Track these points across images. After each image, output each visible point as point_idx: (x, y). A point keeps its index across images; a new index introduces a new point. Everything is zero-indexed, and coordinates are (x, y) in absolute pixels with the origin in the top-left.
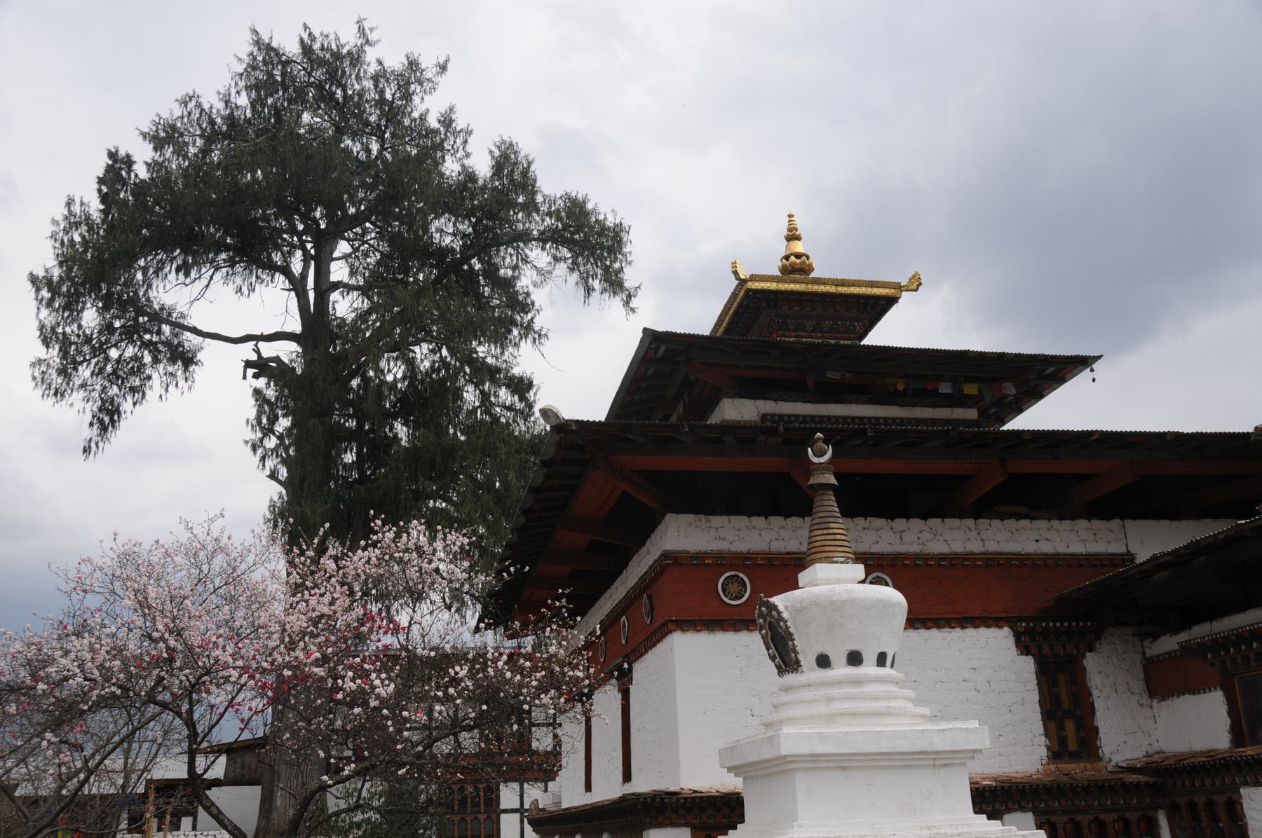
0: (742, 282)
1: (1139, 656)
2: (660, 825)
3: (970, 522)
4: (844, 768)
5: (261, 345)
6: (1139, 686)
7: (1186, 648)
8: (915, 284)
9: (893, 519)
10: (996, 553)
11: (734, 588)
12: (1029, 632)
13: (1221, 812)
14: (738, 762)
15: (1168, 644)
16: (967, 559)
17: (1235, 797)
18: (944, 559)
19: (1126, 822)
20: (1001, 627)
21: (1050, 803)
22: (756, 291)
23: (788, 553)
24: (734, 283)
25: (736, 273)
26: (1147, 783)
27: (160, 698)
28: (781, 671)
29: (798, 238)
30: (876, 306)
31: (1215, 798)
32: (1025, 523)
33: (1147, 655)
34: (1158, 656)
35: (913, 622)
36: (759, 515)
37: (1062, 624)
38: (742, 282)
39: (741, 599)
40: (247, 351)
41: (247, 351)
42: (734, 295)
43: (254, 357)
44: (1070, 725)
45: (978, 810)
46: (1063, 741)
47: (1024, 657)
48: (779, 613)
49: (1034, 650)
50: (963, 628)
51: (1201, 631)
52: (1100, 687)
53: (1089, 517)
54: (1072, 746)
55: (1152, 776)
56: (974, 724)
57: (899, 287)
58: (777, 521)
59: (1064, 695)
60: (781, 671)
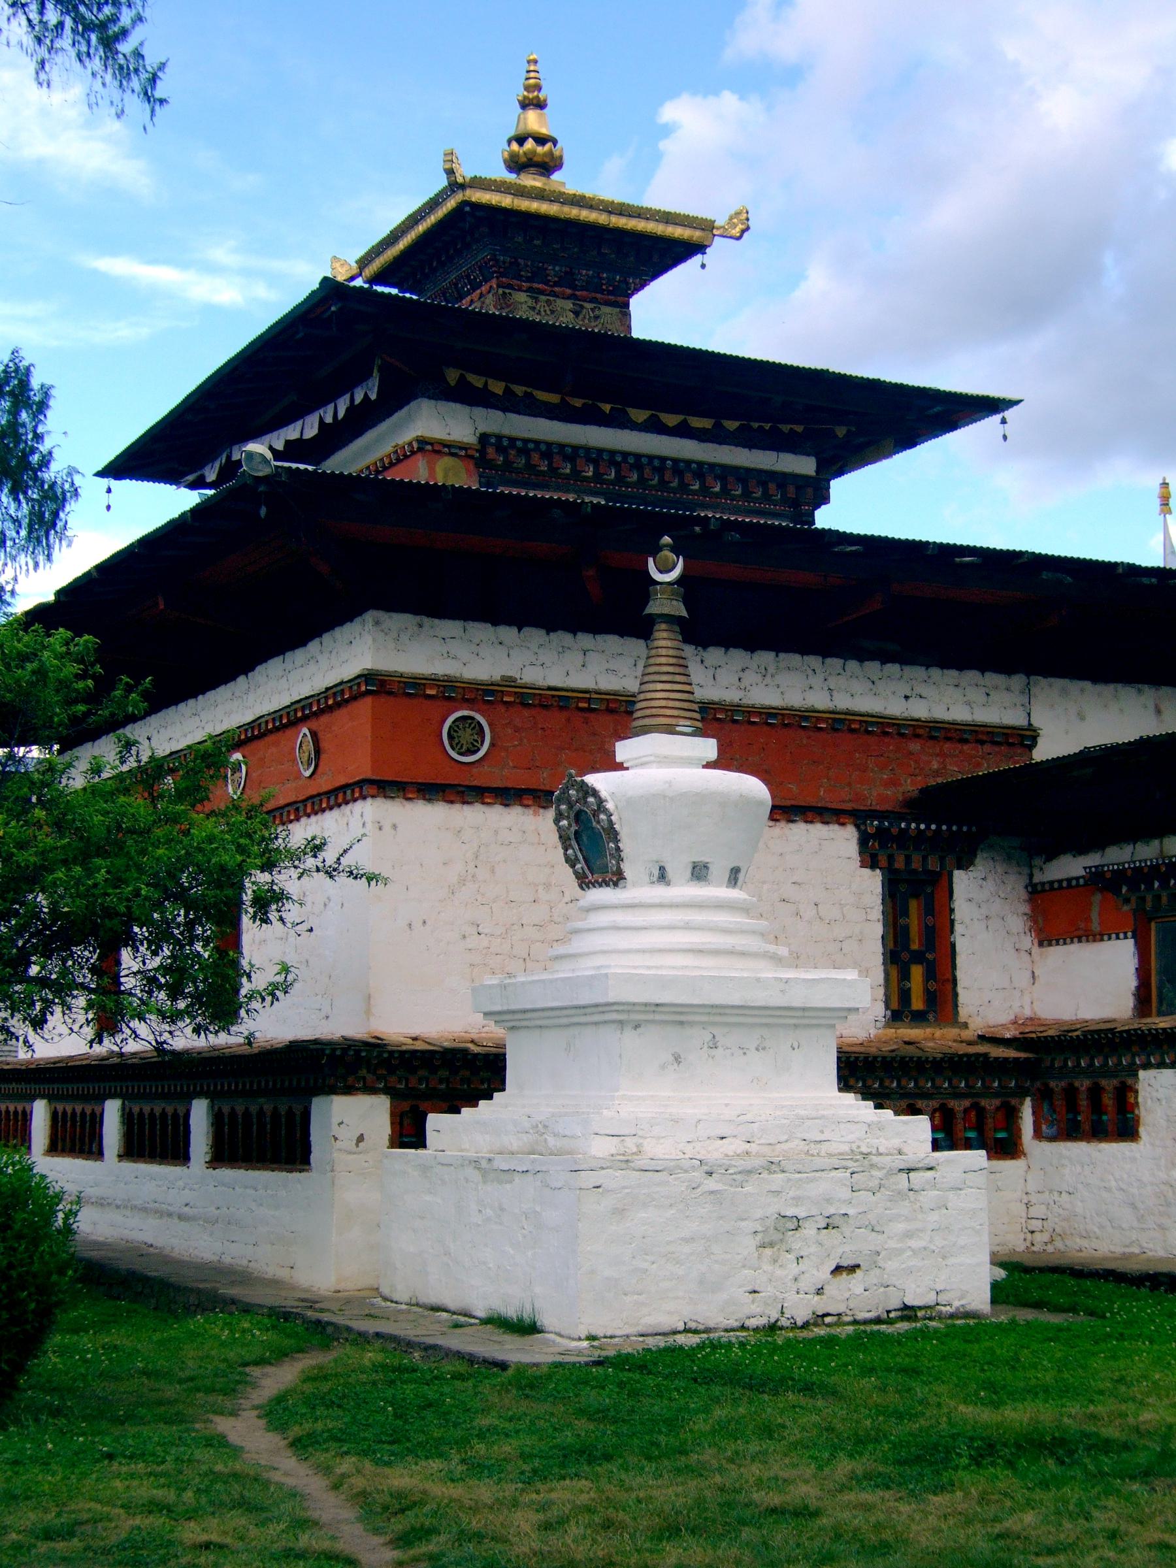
0: (455, 186)
1: (1024, 880)
2: (349, 1090)
4: (681, 1023)
6: (1017, 922)
7: (1097, 880)
8: (740, 227)
9: (705, 647)
10: (848, 713)
11: (466, 736)
12: (881, 834)
13: (1108, 1100)
14: (498, 1008)
15: (1070, 867)
16: (806, 718)
17: (1130, 1081)
18: (774, 716)
19: (981, 1112)
21: (887, 1083)
22: (477, 206)
23: (550, 688)
24: (442, 182)
25: (450, 172)
28: (584, 883)
29: (540, 105)
30: (658, 250)
31: (1104, 1083)
32: (893, 668)
33: (1036, 880)
34: (1051, 883)
36: (509, 623)
37: (928, 827)
39: (536, 760)
44: (917, 972)
45: (845, 1084)
46: (905, 996)
47: (867, 872)
49: (883, 861)
51: (1118, 856)
52: (967, 921)
54: (917, 1004)
55: (1025, 1051)
56: (851, 975)
57: (708, 226)
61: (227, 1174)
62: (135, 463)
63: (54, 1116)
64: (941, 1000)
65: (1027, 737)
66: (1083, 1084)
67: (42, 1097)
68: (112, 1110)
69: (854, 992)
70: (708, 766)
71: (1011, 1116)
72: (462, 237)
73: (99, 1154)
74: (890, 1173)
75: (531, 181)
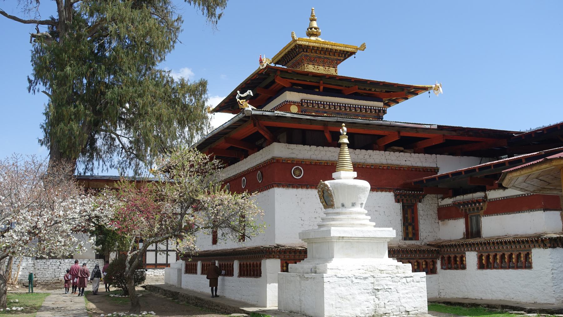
1: (437, 205)
2: (270, 258)
3: (383, 152)
5: (40, 27)
6: (435, 216)
7: (454, 203)
8: (363, 47)
10: (391, 164)
11: (297, 172)
12: (400, 194)
15: (448, 201)
20: (390, 192)
22: (299, 45)
26: (435, 250)
27: (233, 223)
31: (457, 255)
35: (372, 189)
38: (295, 41)
39: (315, 176)
40: (31, 29)
41: (31, 29)
42: (290, 45)
43: (35, 33)
44: (410, 228)
48: (328, 188)
50: (377, 191)
51: (459, 198)
53: (425, 153)
58: (314, 147)
59: (409, 217)
60: (326, 207)
61: (242, 279)
62: (221, 108)
63: (240, 265)
64: (415, 236)
65: (436, 170)
66: (452, 256)
67: (236, 259)
68: (199, 264)
69: (391, 233)
70: (355, 178)
71: (434, 263)
72: (294, 53)
73: (196, 273)
74: (401, 278)
75: (313, 38)
